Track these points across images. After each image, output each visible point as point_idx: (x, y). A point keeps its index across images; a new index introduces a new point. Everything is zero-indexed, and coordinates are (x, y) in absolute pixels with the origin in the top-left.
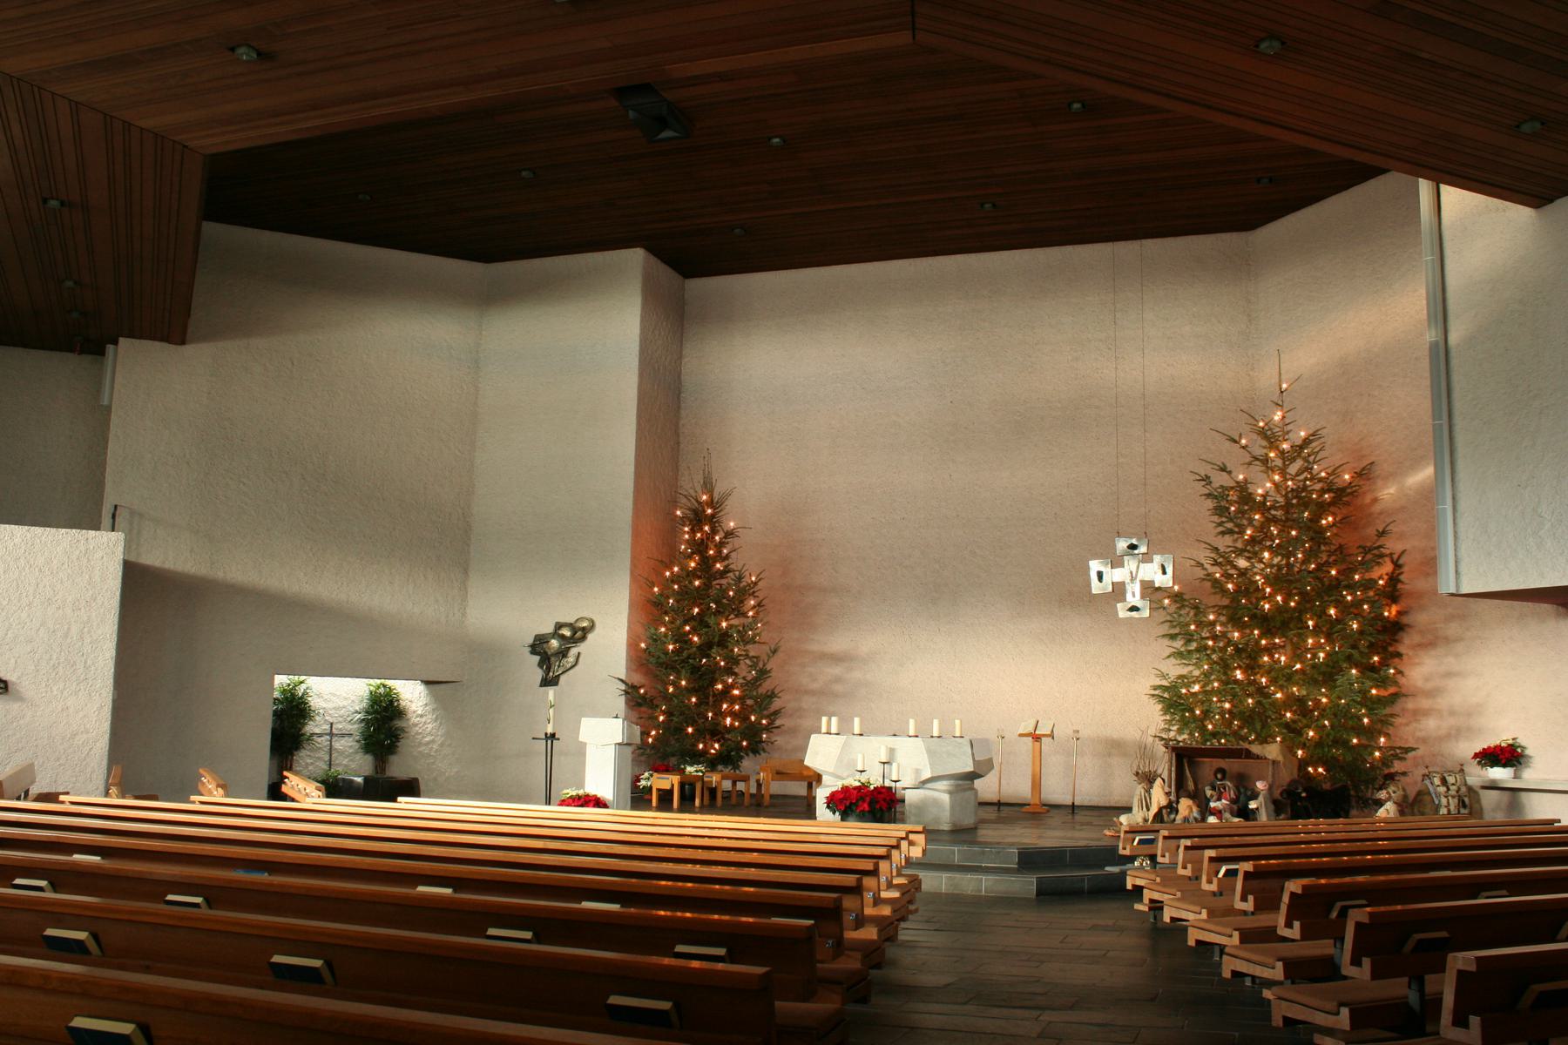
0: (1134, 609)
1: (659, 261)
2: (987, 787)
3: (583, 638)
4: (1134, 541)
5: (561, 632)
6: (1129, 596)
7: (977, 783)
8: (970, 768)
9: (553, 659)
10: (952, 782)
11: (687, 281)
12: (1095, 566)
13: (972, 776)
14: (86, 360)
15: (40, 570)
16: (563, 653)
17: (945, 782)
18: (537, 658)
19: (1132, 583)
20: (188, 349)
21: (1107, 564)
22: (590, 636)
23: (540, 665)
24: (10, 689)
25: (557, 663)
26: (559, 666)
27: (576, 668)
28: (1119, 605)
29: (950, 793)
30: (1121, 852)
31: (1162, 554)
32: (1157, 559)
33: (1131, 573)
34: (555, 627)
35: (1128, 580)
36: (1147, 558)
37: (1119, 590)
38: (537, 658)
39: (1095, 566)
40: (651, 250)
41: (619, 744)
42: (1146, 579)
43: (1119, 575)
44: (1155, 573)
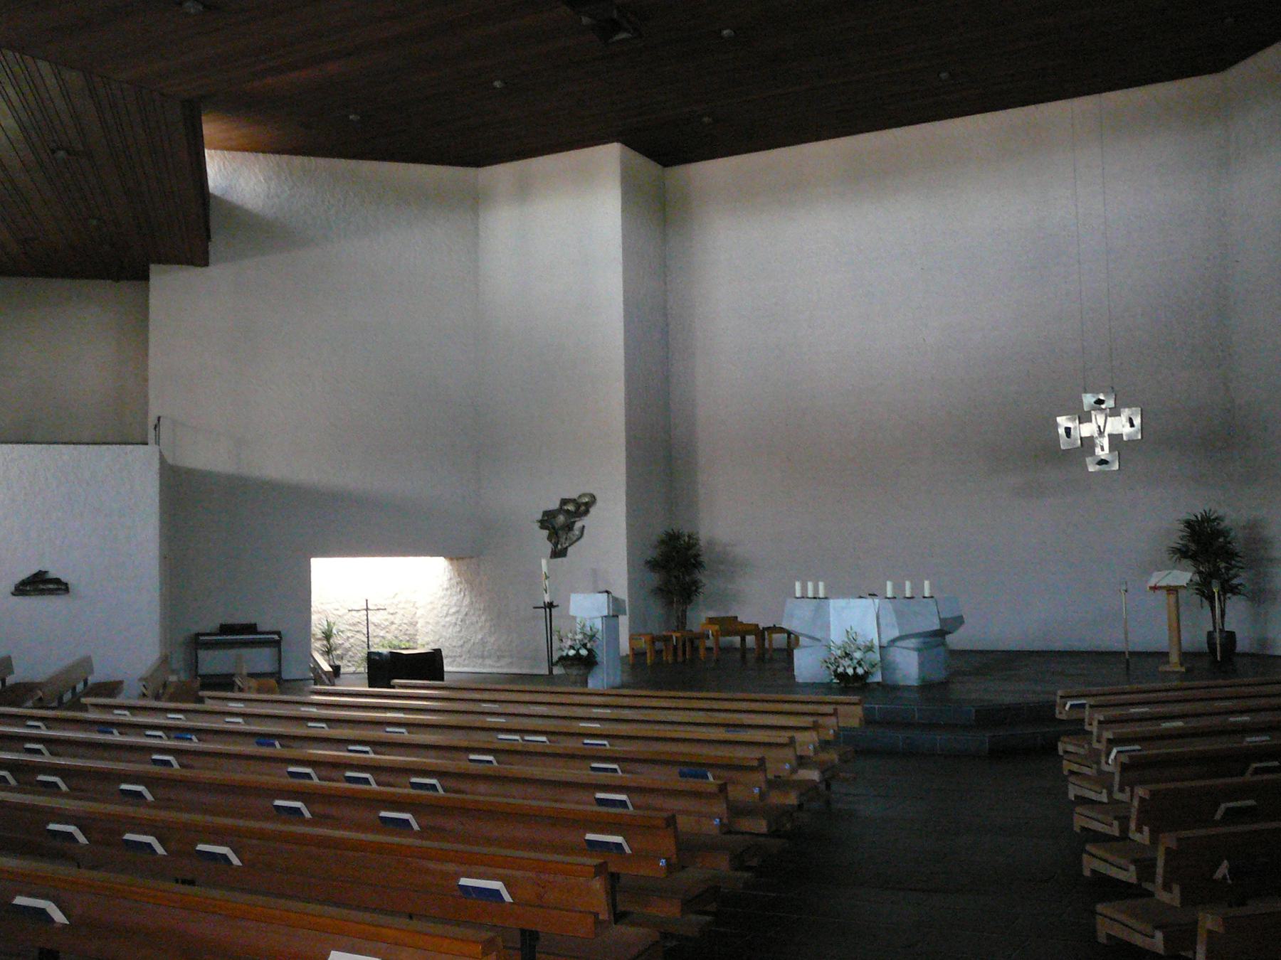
0: (1103, 462)
1: (993, 113)
2: (956, 640)
3: (587, 512)
4: (1102, 397)
5: (566, 508)
6: (1098, 450)
7: (949, 638)
8: (937, 626)
9: (560, 532)
10: (921, 640)
11: (669, 170)
12: (1063, 422)
13: (941, 634)
14: (125, 289)
15: (88, 484)
16: (569, 527)
17: (913, 640)
18: (546, 533)
19: (1100, 437)
20: (213, 271)
21: (1075, 420)
22: (593, 510)
23: (549, 538)
24: (70, 590)
25: (564, 537)
26: (566, 539)
27: (582, 540)
28: (1089, 460)
29: (918, 650)
30: (1058, 716)
31: (1129, 407)
32: (1126, 413)
33: (1099, 427)
34: (561, 503)
35: (1096, 435)
36: (1115, 412)
37: (1088, 444)
38: (546, 533)
39: (1063, 422)
40: (627, 143)
41: (605, 617)
42: (1115, 433)
43: (1087, 430)
44: (1123, 426)
